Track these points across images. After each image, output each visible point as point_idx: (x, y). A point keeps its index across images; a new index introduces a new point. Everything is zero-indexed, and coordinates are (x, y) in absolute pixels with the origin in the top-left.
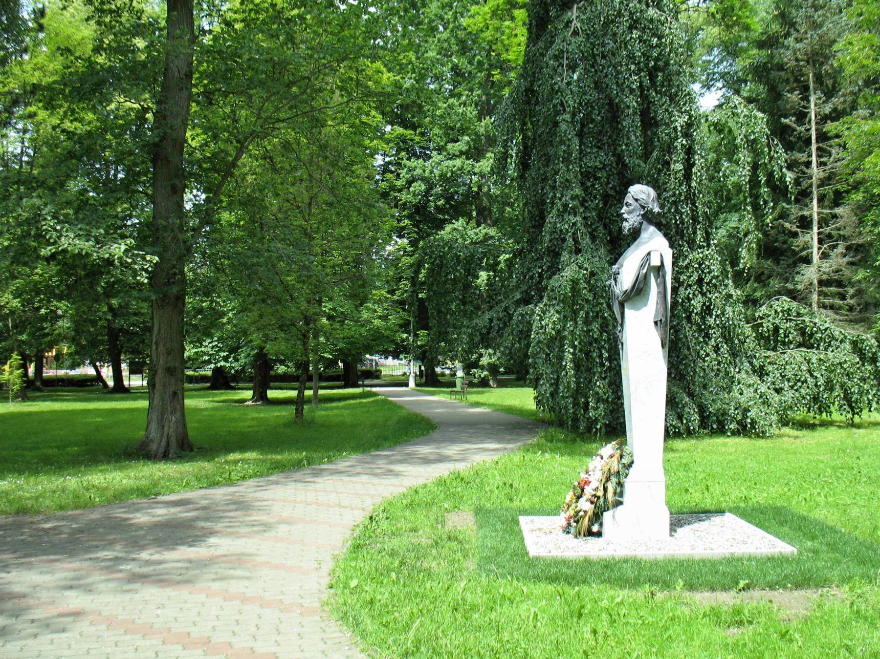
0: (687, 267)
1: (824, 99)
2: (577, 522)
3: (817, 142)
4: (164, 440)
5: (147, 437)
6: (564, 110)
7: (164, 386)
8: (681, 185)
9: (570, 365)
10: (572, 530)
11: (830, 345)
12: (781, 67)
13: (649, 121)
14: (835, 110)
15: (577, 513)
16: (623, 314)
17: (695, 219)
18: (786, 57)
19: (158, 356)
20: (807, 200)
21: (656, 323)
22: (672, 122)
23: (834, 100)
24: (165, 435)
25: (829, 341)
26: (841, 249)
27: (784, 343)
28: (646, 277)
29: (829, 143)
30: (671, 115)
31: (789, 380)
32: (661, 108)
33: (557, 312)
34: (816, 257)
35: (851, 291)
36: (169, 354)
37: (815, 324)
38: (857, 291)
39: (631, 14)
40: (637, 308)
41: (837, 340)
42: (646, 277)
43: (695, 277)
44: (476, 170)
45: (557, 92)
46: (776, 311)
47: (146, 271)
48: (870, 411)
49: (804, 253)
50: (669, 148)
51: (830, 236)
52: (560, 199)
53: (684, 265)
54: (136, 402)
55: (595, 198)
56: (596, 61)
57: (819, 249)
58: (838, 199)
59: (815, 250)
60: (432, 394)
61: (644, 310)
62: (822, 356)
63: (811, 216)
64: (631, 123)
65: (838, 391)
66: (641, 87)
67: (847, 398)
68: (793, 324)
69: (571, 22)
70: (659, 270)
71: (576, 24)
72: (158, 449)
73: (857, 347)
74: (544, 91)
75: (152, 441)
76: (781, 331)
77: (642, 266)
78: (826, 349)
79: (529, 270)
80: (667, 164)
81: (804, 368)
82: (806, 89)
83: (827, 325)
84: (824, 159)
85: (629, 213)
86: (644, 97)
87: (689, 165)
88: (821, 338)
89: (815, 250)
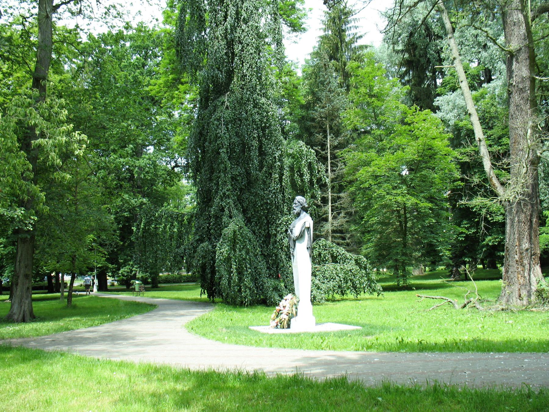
0: (280, 224)
1: (334, 138)
2: (281, 324)
3: (331, 159)
4: (22, 313)
5: (12, 312)
6: (223, 147)
7: (23, 284)
8: (277, 184)
9: (235, 271)
10: (279, 327)
11: (345, 261)
12: (313, 120)
13: (262, 153)
14: (339, 144)
15: (281, 320)
16: (295, 246)
17: (283, 200)
18: (316, 115)
19: (20, 268)
20: (325, 188)
21: (308, 248)
22: (273, 154)
23: (340, 138)
24: (22, 311)
25: (345, 260)
26: (342, 215)
27: (323, 261)
28: (304, 231)
29: (336, 160)
31: (327, 279)
32: (270, 147)
33: (228, 246)
34: (330, 218)
35: (348, 236)
36: (26, 267)
38: (351, 235)
39: (254, 100)
42: (304, 231)
43: (284, 229)
44: (137, 165)
45: (219, 137)
46: (320, 246)
47: (31, 224)
48: (365, 292)
49: (325, 216)
50: (271, 167)
51: (337, 208)
52: (221, 190)
55: (236, 190)
56: (235, 122)
57: (332, 214)
58: (341, 189)
59: (330, 215)
60: (118, 294)
61: (303, 243)
62: (342, 267)
63: (328, 197)
64: (254, 154)
65: (349, 283)
66: (259, 137)
67: (355, 287)
68: (327, 252)
69: (225, 102)
70: (308, 228)
71: (227, 103)
72: (18, 318)
73: (357, 263)
74: (211, 135)
75: (15, 314)
76: (322, 255)
77: (303, 227)
78: (343, 263)
79: (202, 225)
80: (271, 174)
81: (334, 272)
82: (325, 131)
83: (343, 252)
84: (335, 169)
85: (296, 207)
86: (260, 141)
87: (281, 175)
89: (330, 215)
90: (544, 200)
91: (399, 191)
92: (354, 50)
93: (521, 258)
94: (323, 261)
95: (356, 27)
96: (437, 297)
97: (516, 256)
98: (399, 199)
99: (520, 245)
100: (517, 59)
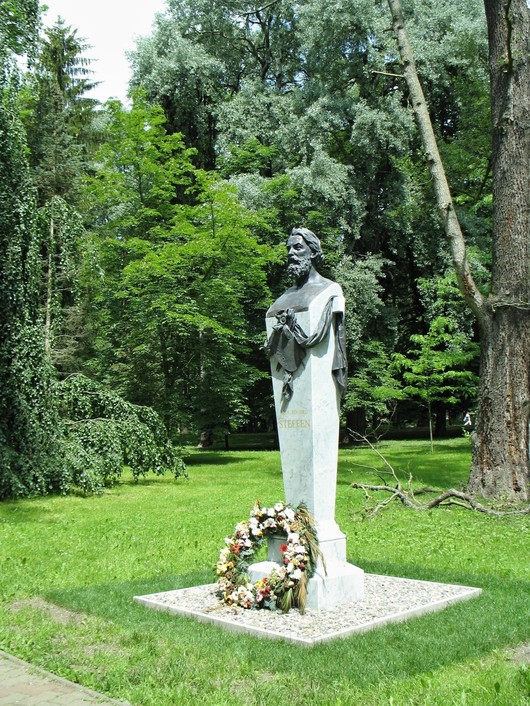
0: (19, 341)
11: (120, 416)
25: (119, 413)
27: (80, 413)
30: (14, 202)
31: (93, 445)
37: (107, 398)
40: (320, 355)
41: (126, 412)
46: (75, 386)
53: (17, 338)
54: (227, 453)
76: (79, 403)
83: (117, 399)
88: (112, 410)
90: (355, 341)
91: (185, 306)
92: (78, 104)
93: (516, 418)
94: (80, 413)
95: (85, 71)
96: (378, 487)
97: (507, 414)
98: (188, 318)
99: (513, 396)
100: (517, 80)
